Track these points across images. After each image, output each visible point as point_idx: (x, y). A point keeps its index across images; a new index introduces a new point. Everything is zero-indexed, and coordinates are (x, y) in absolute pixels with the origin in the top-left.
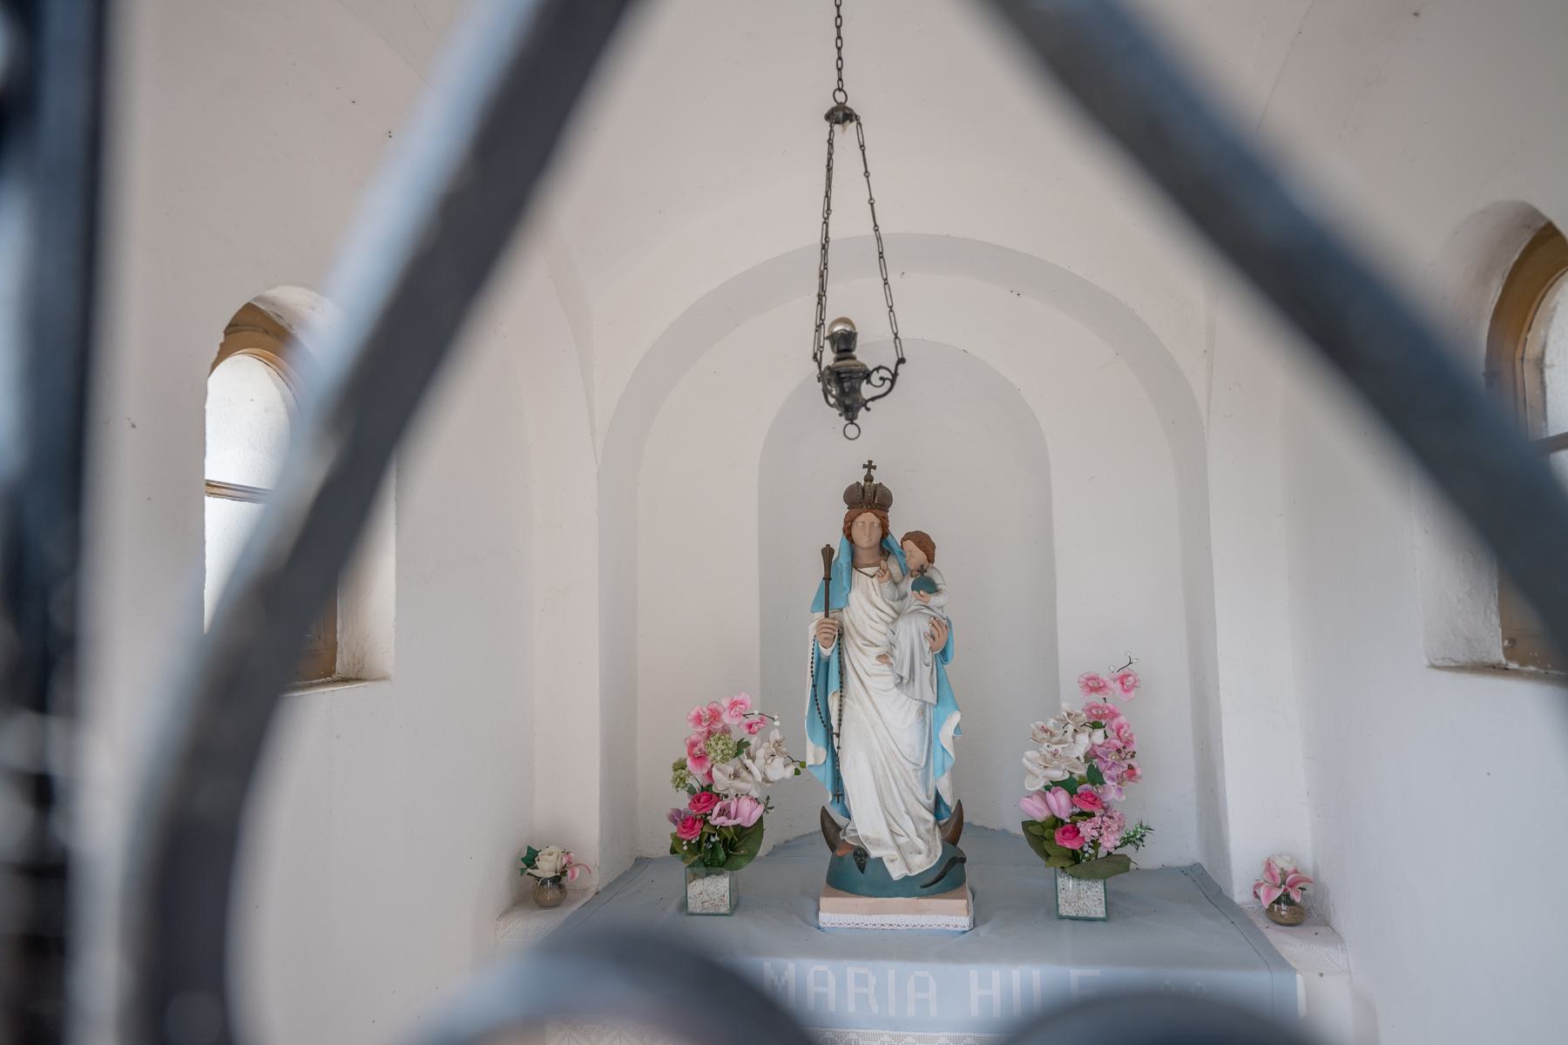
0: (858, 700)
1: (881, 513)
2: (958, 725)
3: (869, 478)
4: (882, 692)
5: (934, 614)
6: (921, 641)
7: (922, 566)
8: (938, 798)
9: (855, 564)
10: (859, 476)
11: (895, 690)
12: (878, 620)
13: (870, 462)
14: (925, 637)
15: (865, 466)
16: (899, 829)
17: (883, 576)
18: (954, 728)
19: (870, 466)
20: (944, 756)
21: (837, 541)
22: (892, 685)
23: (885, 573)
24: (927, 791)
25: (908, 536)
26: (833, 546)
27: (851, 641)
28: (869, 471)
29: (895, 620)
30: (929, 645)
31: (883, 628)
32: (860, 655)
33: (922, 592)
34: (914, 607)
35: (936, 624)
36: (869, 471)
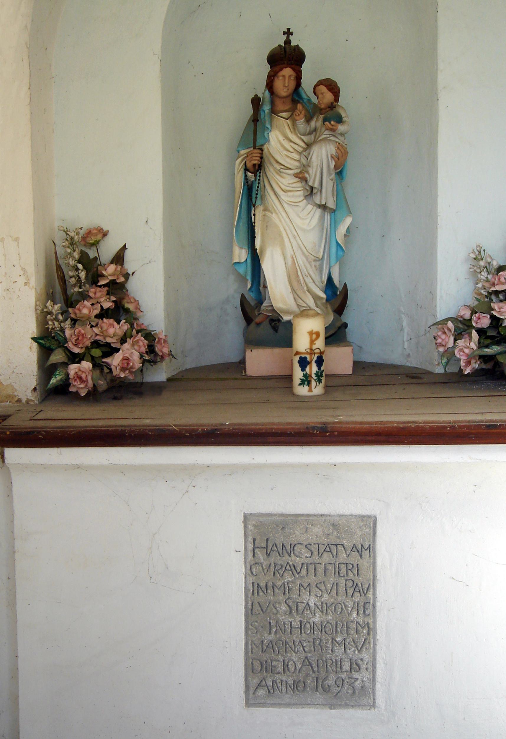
0: (275, 210)
1: (297, 68)
2: (348, 227)
3: (288, 42)
4: (293, 204)
5: (339, 141)
6: (328, 160)
7: (332, 103)
8: (330, 279)
9: (274, 111)
10: (281, 40)
11: (305, 201)
12: (291, 150)
13: (289, 29)
14: (332, 157)
15: (284, 33)
16: (302, 302)
17: (299, 115)
18: (346, 229)
19: (288, 33)
20: (307, 304)
21: (261, 91)
22: (302, 198)
23: (301, 113)
24: (321, 278)
25: (320, 83)
26: (260, 95)
27: (269, 165)
28: (288, 37)
29: (309, 146)
30: (334, 163)
31: (296, 156)
32: (278, 177)
33: (332, 123)
34: (324, 136)
35: (340, 147)
36: (288, 37)
